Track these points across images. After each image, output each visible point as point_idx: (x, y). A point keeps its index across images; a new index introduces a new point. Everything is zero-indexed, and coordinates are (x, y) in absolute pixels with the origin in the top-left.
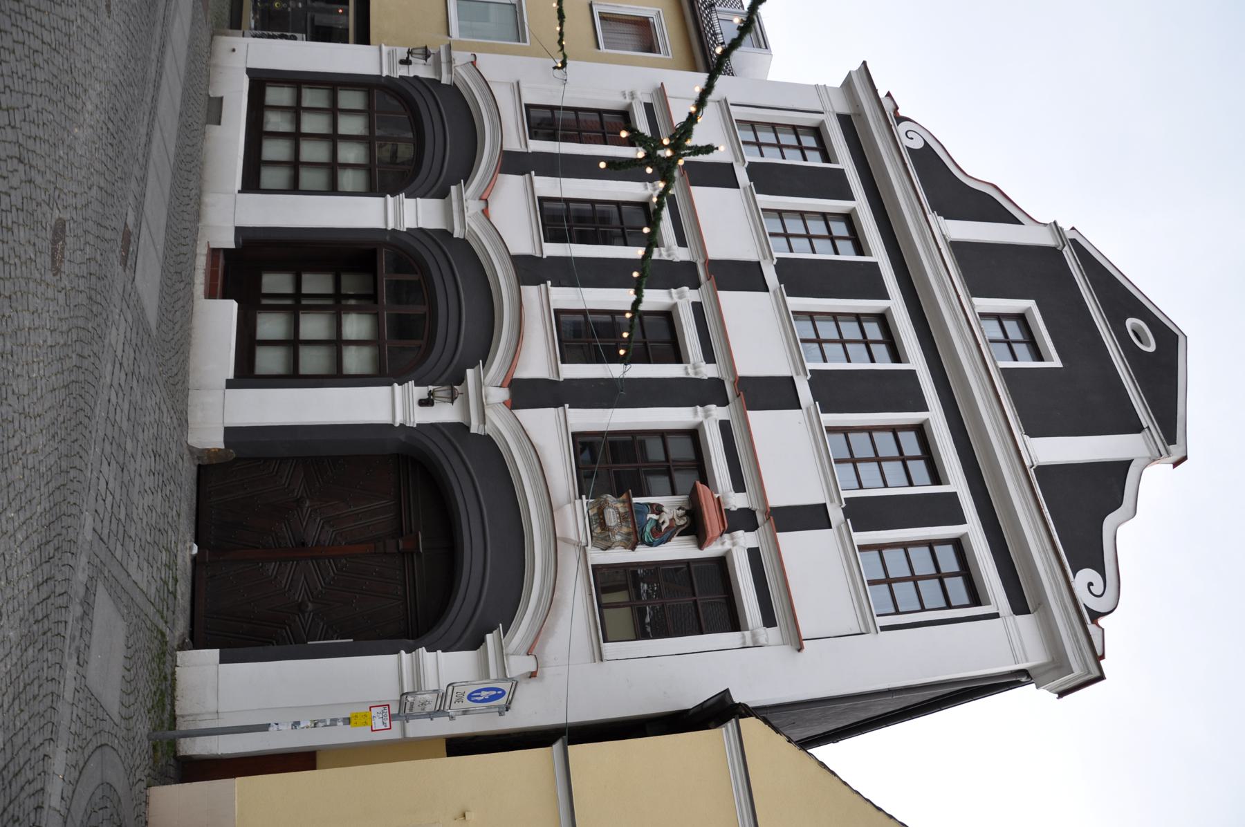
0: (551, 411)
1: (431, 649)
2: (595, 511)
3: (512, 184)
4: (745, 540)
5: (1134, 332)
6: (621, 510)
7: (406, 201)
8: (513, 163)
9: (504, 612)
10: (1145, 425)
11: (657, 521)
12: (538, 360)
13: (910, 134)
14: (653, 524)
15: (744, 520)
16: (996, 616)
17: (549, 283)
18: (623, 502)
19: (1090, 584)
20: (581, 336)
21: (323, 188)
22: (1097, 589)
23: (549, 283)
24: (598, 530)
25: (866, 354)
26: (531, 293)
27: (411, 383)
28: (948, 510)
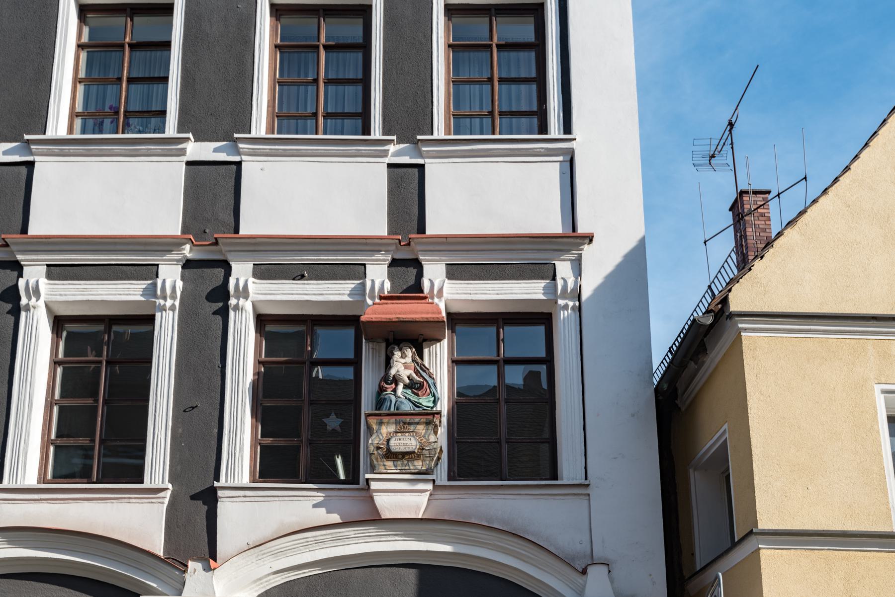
0: (219, 504)
2: (389, 463)
6: (392, 428)
11: (406, 387)
12: (136, 518)
14: (409, 391)
15: (408, 269)
17: (216, 484)
18: (381, 424)
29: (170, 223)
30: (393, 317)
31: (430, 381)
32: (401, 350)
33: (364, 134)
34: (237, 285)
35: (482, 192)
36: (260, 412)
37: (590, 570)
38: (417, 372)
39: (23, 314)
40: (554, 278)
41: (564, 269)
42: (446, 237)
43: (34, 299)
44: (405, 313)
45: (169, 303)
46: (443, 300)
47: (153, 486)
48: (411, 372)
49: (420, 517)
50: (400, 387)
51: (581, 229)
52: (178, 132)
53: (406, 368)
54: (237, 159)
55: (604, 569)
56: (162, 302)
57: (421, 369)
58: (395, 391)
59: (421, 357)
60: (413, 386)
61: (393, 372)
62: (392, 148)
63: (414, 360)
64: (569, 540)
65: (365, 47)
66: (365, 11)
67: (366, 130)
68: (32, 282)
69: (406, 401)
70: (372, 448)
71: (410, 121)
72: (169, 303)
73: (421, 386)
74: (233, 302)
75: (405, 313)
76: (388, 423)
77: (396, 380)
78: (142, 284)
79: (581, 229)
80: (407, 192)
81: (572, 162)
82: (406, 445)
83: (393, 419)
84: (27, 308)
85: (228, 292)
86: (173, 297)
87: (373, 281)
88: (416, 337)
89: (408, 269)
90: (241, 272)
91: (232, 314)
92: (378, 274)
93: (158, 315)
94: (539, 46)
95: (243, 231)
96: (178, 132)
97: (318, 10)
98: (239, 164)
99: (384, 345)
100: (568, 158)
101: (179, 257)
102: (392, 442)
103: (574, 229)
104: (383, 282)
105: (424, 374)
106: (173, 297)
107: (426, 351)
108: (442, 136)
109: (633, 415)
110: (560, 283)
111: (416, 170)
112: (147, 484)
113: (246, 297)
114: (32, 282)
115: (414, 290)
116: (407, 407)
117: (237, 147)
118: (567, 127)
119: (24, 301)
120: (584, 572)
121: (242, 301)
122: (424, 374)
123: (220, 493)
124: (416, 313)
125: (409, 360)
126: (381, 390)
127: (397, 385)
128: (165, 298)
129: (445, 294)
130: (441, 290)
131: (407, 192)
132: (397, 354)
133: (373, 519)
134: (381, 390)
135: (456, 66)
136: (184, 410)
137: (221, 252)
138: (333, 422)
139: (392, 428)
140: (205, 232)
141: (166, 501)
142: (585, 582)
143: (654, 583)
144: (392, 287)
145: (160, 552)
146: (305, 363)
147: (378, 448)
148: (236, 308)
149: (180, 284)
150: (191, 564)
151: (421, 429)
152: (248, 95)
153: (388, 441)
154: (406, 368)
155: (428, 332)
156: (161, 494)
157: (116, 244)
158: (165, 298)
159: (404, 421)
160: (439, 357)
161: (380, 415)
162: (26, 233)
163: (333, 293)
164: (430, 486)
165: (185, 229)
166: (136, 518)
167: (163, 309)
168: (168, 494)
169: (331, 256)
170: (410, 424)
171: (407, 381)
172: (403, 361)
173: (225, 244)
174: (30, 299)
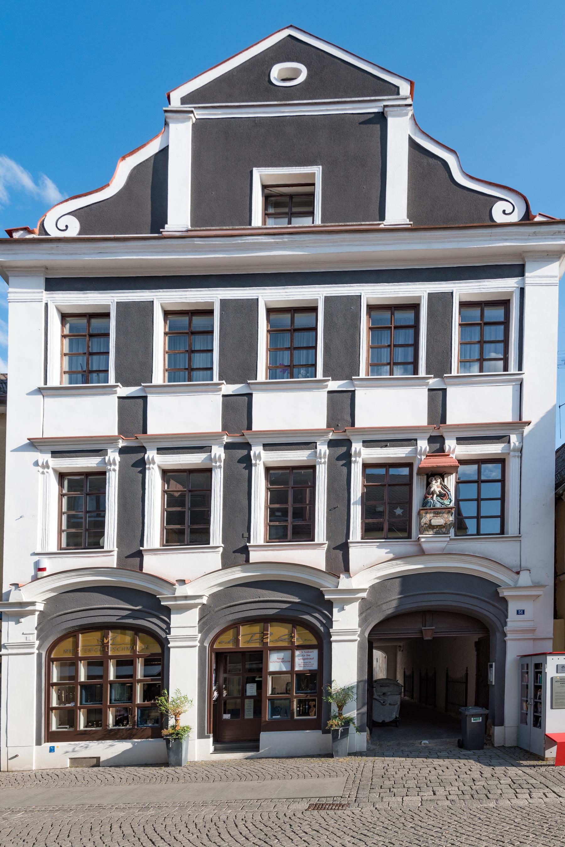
0: (350, 549)
1: (505, 624)
3: (153, 564)
4: (450, 444)
5: (284, 80)
7: (172, 634)
8: (133, 555)
9: (490, 591)
10: (380, 110)
12: (312, 556)
13: (62, 226)
14: (439, 498)
15: (437, 441)
16: (522, 290)
17: (141, 548)
18: (426, 513)
19: (504, 212)
20: (291, 521)
21: (314, 333)
22: (509, 209)
23: (141, 548)
24: (444, 530)
25: (306, 334)
26: (255, 556)
27: (168, 637)
28: (441, 302)
29: (321, 423)
30: (434, 465)
31: (449, 493)
32: (435, 479)
33: (414, 374)
34: (356, 451)
35: (475, 402)
36: (269, 477)
37: (521, 572)
38: (442, 489)
39: (253, 468)
40: (509, 442)
41: (514, 438)
42: (458, 425)
43: (258, 461)
44: (440, 463)
45: (323, 460)
46: (454, 455)
47: (319, 542)
48: (440, 489)
49: (115, 566)
50: (435, 496)
51: (524, 419)
52: (324, 377)
53: (438, 487)
54: (353, 389)
55: (528, 572)
56: (320, 460)
57: (444, 487)
58: (432, 498)
59: (444, 481)
60: (441, 495)
61: (432, 489)
62: (431, 381)
63: (441, 484)
64: (511, 560)
65: (416, 327)
66: (415, 307)
67: (416, 372)
68: (257, 453)
69: (438, 503)
70: (422, 524)
71: (439, 366)
72: (323, 460)
73: (445, 495)
74: (353, 459)
75: (440, 463)
76: (430, 513)
77: (433, 493)
78: (308, 452)
79: (524, 419)
80: (438, 403)
81: (521, 385)
82: (439, 522)
83: (433, 511)
84: (256, 465)
85: (351, 454)
86: (115, 464)
87: (421, 447)
88: (440, 473)
89: (437, 441)
90: (357, 446)
91: (353, 465)
92: (423, 444)
93: (317, 467)
94: (506, 323)
95: (357, 425)
96: (324, 377)
97: (391, 307)
98: (354, 391)
99: (425, 477)
100: (520, 383)
101: (327, 438)
102: (432, 521)
103: (520, 419)
104: (426, 447)
105: (446, 490)
106: (325, 458)
107: (446, 479)
108: (456, 374)
109: (544, 505)
110: (512, 445)
111: (441, 392)
112: (316, 541)
113: (360, 457)
114: (257, 453)
115: (441, 451)
116: (438, 505)
117: (353, 383)
118: (520, 368)
119: (253, 462)
120: (518, 573)
121: (358, 459)
122: (446, 490)
123: (350, 545)
124: (445, 463)
125: (439, 483)
126: (426, 498)
127: (433, 495)
128: (321, 458)
129: (456, 452)
130: (454, 450)
131: (438, 403)
132: (434, 482)
133: (422, 553)
134: (426, 498)
135: (462, 335)
136: (331, 509)
137: (346, 435)
138: (399, 511)
139: (432, 515)
140: (338, 426)
141: (326, 549)
142: (519, 578)
143: (548, 577)
144: (430, 449)
145: (323, 568)
146: (385, 485)
147: (426, 524)
148: (355, 461)
149: (327, 451)
150: (342, 576)
151: (446, 516)
152: (358, 356)
153: (430, 521)
154: (438, 487)
155: (447, 470)
156: (324, 546)
157: (297, 433)
158: (321, 458)
159: (437, 512)
160: (451, 481)
161: (426, 509)
162: (251, 429)
163: (398, 453)
164: (448, 539)
165: (329, 425)
166: (312, 556)
167: (320, 463)
168: (326, 546)
169: (402, 437)
170: (440, 513)
171: (438, 493)
172: (436, 484)
173: (349, 432)
174: (256, 461)
